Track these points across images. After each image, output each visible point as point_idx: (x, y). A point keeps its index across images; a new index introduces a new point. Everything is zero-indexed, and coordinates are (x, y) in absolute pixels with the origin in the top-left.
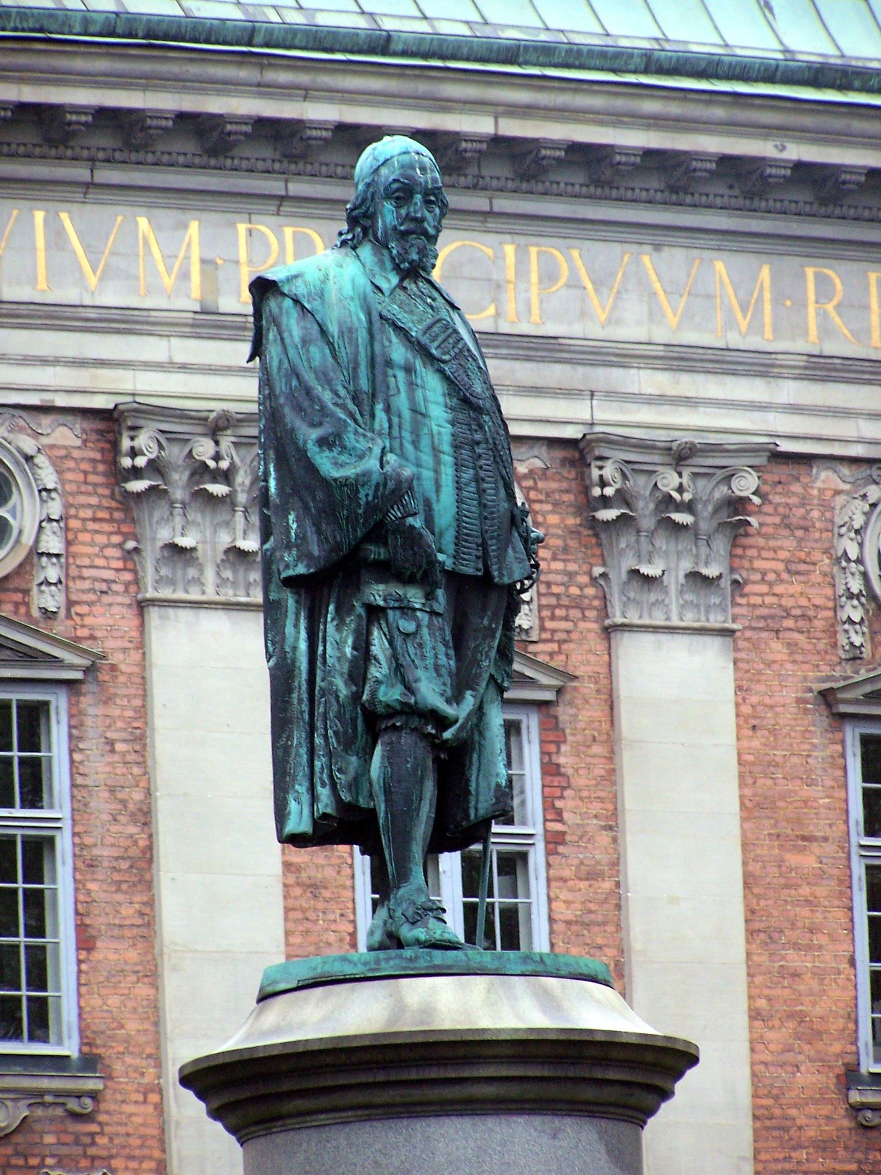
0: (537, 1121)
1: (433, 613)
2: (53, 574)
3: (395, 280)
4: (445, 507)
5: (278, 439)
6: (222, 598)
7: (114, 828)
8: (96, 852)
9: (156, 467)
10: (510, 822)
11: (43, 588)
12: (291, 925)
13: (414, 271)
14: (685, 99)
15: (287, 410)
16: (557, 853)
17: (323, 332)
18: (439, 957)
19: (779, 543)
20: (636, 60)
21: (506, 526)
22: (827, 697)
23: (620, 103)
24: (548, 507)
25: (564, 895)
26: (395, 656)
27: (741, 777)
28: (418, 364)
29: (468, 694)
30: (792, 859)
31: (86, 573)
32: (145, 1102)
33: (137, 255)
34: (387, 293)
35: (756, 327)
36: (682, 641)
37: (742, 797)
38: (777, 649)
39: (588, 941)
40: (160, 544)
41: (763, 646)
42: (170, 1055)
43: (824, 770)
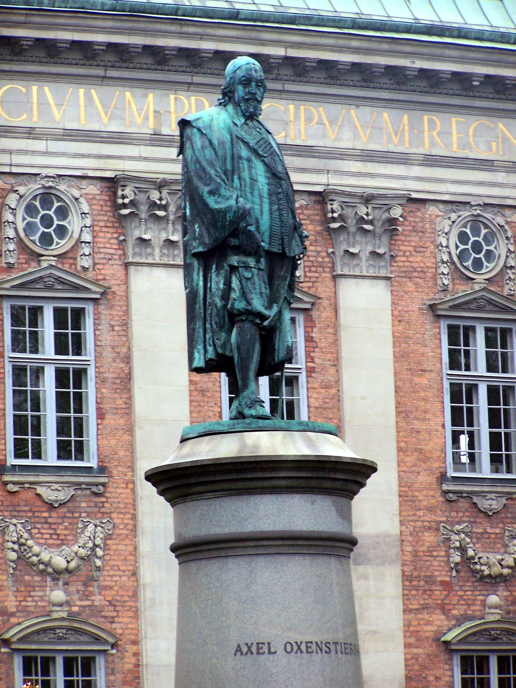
0: (305, 497)
1: (259, 269)
2: (87, 251)
3: (243, 120)
4: (265, 221)
5: (190, 191)
6: (162, 262)
7: (114, 365)
8: (106, 375)
9: (133, 203)
10: (291, 363)
11: (83, 257)
12: (193, 408)
13: (251, 116)
14: (370, 40)
15: (194, 178)
16: (312, 377)
17: (211, 143)
18: (261, 423)
19: (411, 239)
20: (349, 23)
21: (292, 230)
22: (432, 307)
23: (342, 42)
24: (308, 222)
25: (315, 395)
26: (242, 288)
27: (394, 343)
28: (253, 158)
29: (275, 305)
30: (417, 380)
31: (102, 250)
32: (127, 488)
33: (125, 109)
34: (239, 126)
35: (401, 142)
36: (368, 282)
37: (394, 352)
38: (410, 286)
39: (325, 416)
40: (135, 238)
41: (404, 284)
42: (138, 467)
43: (431, 340)
